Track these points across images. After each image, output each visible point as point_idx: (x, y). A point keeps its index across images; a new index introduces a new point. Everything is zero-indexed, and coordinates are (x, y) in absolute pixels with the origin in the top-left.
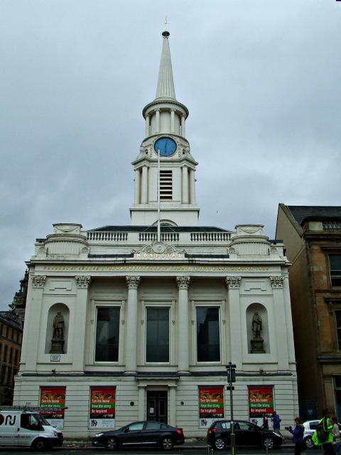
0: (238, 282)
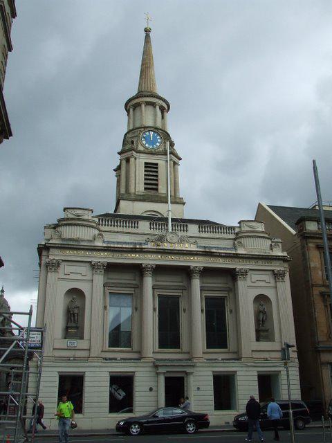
0: (244, 273)
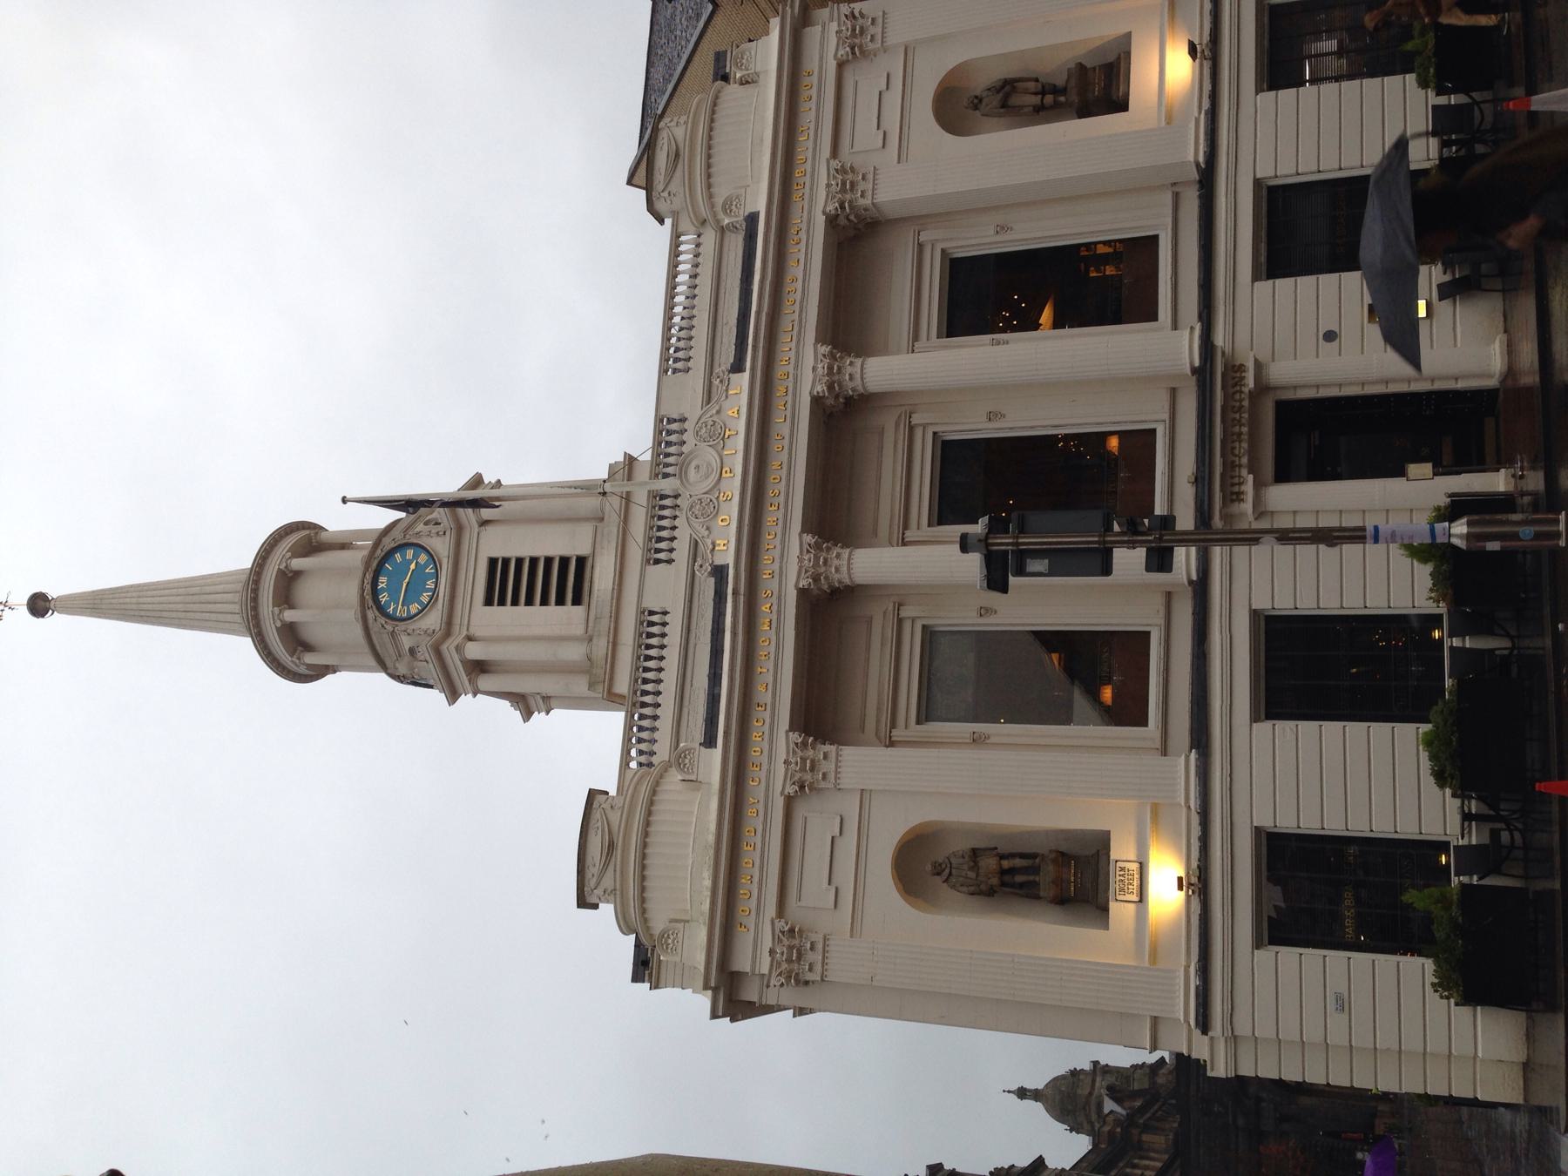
0: (847, 179)
